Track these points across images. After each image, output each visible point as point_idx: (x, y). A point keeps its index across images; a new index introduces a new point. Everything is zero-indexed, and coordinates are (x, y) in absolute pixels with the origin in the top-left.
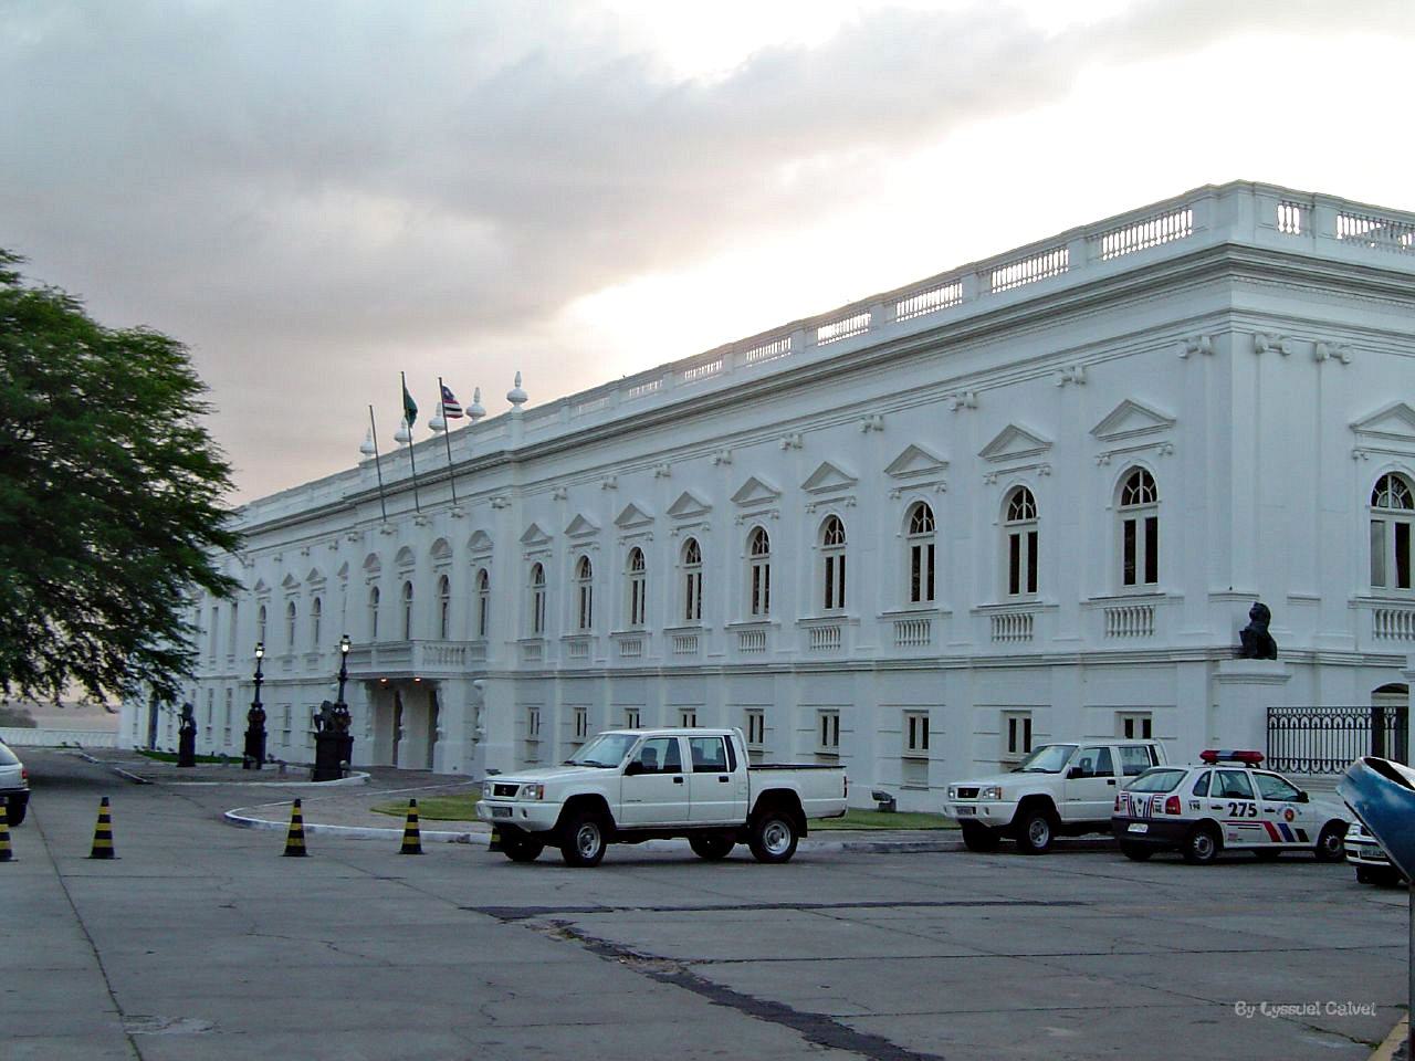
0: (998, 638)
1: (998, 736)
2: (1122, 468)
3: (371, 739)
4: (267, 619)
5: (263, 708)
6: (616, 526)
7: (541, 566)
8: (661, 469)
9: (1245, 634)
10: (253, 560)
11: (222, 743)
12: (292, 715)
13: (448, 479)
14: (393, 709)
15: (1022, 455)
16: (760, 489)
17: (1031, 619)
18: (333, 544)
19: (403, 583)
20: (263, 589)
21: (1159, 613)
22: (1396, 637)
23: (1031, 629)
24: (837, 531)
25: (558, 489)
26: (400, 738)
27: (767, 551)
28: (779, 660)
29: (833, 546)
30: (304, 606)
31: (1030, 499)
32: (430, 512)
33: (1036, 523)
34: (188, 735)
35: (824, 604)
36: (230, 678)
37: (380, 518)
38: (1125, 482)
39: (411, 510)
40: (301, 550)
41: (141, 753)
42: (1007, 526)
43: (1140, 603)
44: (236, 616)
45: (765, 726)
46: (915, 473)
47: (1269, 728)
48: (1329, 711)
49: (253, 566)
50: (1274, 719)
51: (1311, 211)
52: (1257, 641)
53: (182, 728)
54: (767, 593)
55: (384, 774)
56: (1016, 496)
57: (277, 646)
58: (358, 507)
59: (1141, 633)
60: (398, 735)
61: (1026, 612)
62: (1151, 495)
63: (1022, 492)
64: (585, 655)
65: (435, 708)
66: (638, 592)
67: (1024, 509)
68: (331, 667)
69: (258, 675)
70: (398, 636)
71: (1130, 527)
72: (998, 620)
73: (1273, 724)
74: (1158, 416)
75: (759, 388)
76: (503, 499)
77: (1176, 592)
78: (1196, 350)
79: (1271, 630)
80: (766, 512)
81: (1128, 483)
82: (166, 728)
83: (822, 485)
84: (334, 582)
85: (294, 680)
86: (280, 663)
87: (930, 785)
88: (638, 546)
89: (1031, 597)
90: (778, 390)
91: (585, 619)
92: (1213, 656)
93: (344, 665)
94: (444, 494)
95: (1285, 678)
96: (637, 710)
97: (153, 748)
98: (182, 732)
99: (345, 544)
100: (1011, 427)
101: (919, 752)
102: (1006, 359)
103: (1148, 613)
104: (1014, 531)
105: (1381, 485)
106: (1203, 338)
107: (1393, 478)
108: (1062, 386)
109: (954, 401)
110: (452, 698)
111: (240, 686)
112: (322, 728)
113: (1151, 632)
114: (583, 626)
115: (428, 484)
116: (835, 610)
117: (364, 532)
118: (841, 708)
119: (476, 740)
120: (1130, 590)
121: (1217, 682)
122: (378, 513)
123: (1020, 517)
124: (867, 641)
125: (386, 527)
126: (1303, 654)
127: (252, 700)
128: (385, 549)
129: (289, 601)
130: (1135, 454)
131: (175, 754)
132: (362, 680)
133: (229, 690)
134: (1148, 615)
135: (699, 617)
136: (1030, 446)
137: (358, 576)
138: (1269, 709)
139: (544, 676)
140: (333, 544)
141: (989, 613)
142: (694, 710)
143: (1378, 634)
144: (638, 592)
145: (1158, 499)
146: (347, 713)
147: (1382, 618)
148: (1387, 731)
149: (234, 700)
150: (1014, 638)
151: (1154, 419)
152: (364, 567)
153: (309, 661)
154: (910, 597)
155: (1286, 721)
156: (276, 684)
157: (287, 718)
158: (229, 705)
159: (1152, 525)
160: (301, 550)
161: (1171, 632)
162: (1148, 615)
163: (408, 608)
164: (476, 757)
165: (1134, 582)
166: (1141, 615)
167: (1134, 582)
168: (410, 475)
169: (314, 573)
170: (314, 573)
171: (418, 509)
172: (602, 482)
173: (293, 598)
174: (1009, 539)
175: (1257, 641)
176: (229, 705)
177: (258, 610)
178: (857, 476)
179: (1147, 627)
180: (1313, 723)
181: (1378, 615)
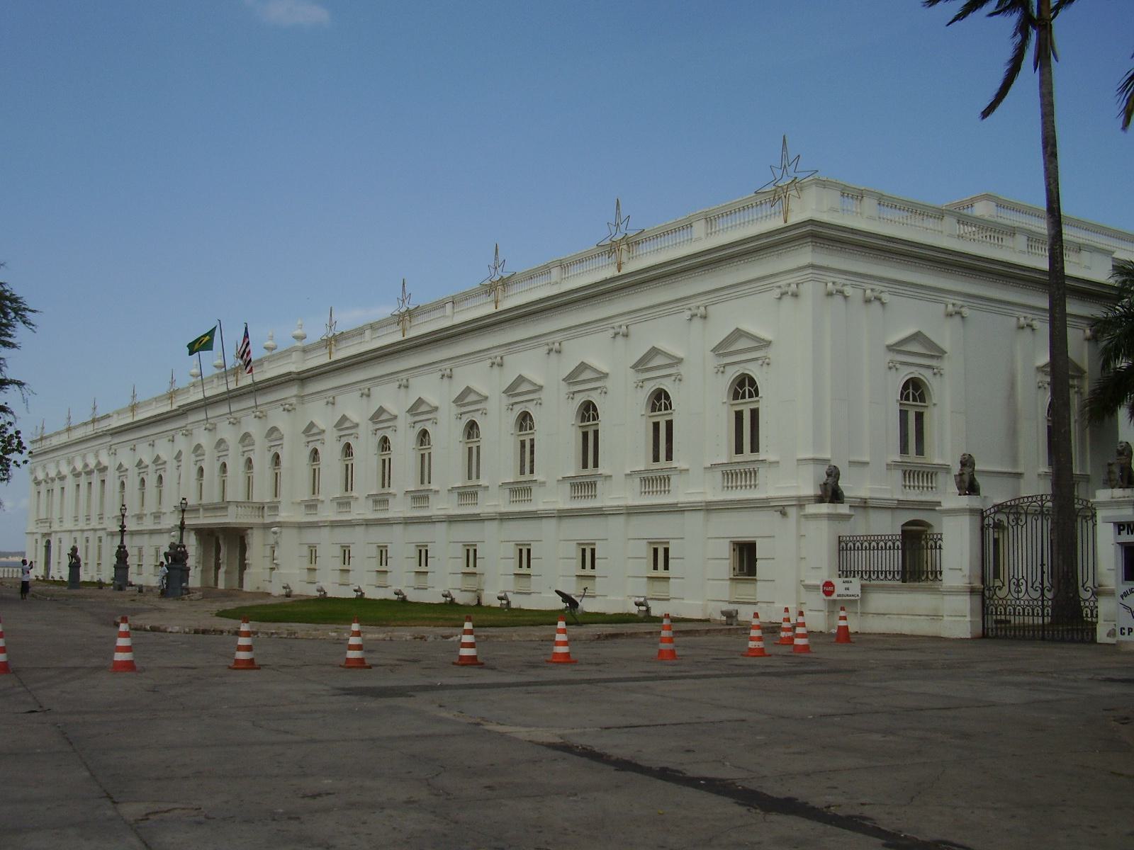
0: (645, 493)
1: (461, 560)
3: (199, 569)
4: (164, 483)
5: (126, 549)
7: (251, 460)
10: (115, 450)
11: (411, 579)
12: (144, 553)
13: (227, 399)
15: (347, 428)
19: (272, 454)
21: (761, 473)
22: (916, 488)
23: (669, 487)
24: (591, 412)
25: (329, 397)
26: (219, 568)
28: (486, 511)
29: (588, 423)
30: (151, 480)
31: (595, 409)
33: (672, 413)
34: (75, 566)
36: (87, 530)
40: (168, 438)
41: (41, 581)
42: (650, 417)
43: (747, 467)
44: (104, 488)
45: (477, 556)
46: (584, 381)
47: (839, 550)
48: (883, 538)
49: (333, 404)
50: (843, 544)
52: (832, 493)
53: (70, 563)
55: (209, 592)
56: (739, 382)
58: (188, 412)
59: (748, 487)
60: (218, 567)
63: (745, 378)
65: (243, 548)
67: (663, 404)
68: (172, 521)
69: (123, 526)
70: (216, 499)
72: (644, 480)
77: (684, 466)
78: (619, 333)
79: (840, 484)
81: (584, 410)
83: (466, 401)
84: (171, 464)
86: (135, 519)
87: (596, 594)
88: (387, 435)
89: (754, 457)
92: (800, 502)
93: (183, 518)
94: (224, 409)
95: (849, 517)
97: (48, 577)
98: (71, 566)
99: (179, 438)
104: (656, 420)
105: (906, 386)
106: (792, 285)
107: (913, 381)
109: (689, 313)
110: (256, 544)
112: (170, 561)
113: (755, 486)
114: (314, 493)
115: (263, 389)
116: (590, 470)
118: (429, 544)
119: (272, 569)
120: (739, 458)
121: (803, 519)
122: (251, 403)
124: (695, 486)
125: (232, 420)
127: (119, 543)
133: (36, 540)
134: (753, 475)
135: (352, 490)
137: (189, 461)
138: (839, 537)
139: (321, 524)
141: (457, 491)
142: (476, 545)
143: (905, 487)
146: (185, 551)
147: (907, 475)
148: (925, 551)
151: (757, 341)
152: (193, 453)
153: (155, 517)
155: (883, 544)
156: (133, 533)
157: (140, 556)
158: (100, 547)
160: (168, 438)
161: (608, 497)
162: (753, 475)
164: (272, 580)
165: (658, 461)
166: (730, 476)
167: (658, 461)
168: (225, 390)
169: (158, 458)
170: (158, 458)
171: (231, 413)
173: (144, 476)
174: (652, 425)
176: (100, 547)
178: (607, 371)
179: (753, 483)
180: (896, 545)
181: (905, 474)
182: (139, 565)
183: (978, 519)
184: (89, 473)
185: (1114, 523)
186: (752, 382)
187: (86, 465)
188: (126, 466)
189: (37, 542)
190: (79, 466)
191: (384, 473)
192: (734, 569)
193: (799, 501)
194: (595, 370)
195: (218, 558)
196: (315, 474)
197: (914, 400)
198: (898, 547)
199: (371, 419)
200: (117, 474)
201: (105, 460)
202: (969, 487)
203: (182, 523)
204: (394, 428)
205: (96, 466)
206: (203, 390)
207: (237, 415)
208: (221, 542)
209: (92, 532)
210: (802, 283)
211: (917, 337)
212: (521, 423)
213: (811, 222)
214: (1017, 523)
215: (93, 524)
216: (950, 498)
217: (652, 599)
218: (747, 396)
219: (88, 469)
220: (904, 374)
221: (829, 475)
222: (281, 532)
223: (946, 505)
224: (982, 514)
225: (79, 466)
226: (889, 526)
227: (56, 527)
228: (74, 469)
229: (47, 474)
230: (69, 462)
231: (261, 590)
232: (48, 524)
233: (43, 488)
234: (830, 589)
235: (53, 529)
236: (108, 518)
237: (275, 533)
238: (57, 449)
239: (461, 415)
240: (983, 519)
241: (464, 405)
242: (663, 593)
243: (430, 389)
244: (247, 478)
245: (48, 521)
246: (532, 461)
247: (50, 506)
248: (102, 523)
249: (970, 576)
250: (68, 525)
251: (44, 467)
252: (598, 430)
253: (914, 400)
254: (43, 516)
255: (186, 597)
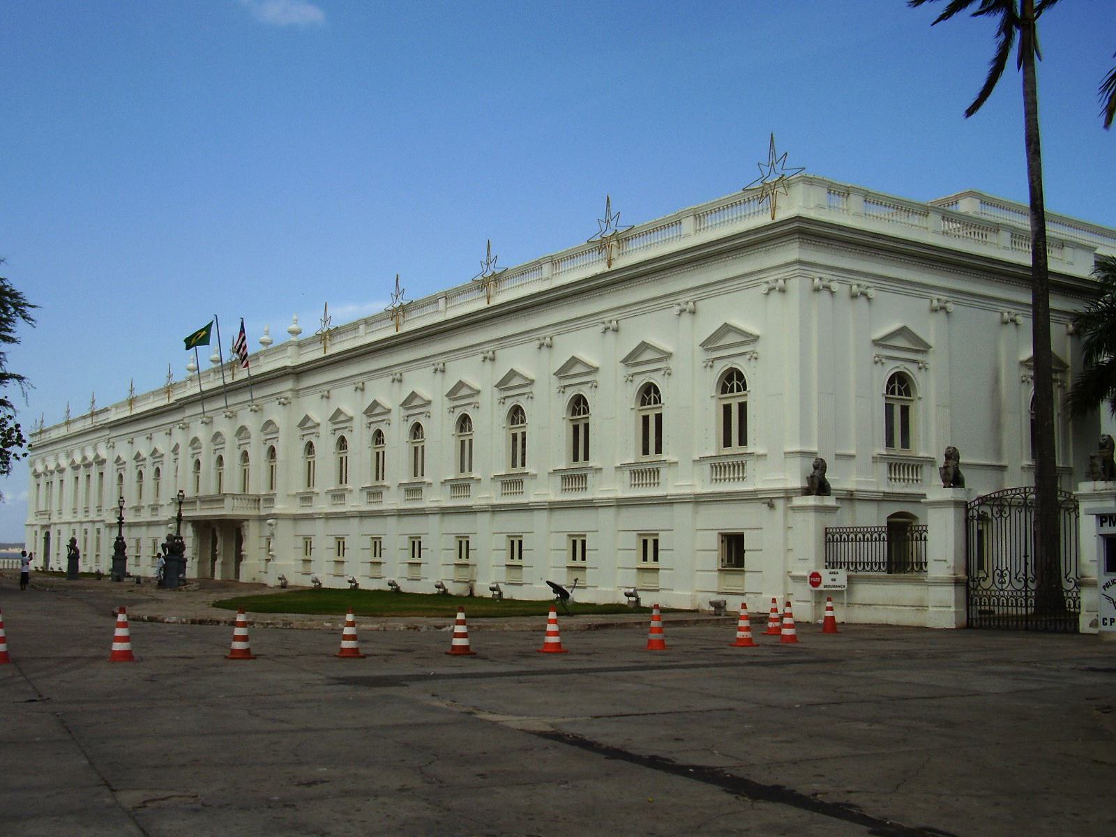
2: (719, 372)
5: (124, 540)
6: (364, 416)
7: (312, 443)
8: (324, 393)
9: (811, 479)
11: (404, 571)
14: (210, 541)
16: (649, 351)
17: (658, 472)
18: (149, 435)
20: (157, 455)
21: (662, 471)
22: (902, 481)
23: (658, 479)
26: (216, 560)
27: (346, 448)
30: (149, 473)
32: (234, 409)
35: (375, 478)
37: (200, 414)
38: (724, 378)
39: (247, 401)
42: (639, 410)
43: (735, 460)
46: (416, 407)
47: (826, 542)
50: (830, 536)
51: (847, 197)
54: (346, 476)
55: (205, 583)
57: (130, 502)
60: (214, 558)
61: (739, 460)
62: (658, 400)
63: (733, 373)
64: (420, 497)
65: (239, 540)
66: (343, 464)
68: (168, 513)
70: (213, 491)
71: (646, 419)
72: (634, 473)
73: (830, 539)
74: (663, 351)
75: (353, 353)
76: (286, 399)
77: (674, 459)
80: (470, 404)
82: (55, 556)
84: (169, 457)
85: (142, 522)
86: (132, 511)
89: (742, 450)
90: (131, 422)
91: (342, 478)
92: (788, 495)
93: (180, 510)
94: (220, 403)
96: (344, 538)
97: (47, 568)
98: (69, 557)
99: (177, 432)
100: (643, 343)
101: (516, 562)
102: (85, 440)
103: (583, 478)
105: (891, 381)
107: (898, 376)
108: (679, 315)
109: (678, 308)
110: (252, 536)
111: (106, 527)
112: (167, 553)
115: (258, 383)
116: (581, 463)
117: (188, 424)
119: (268, 560)
120: (728, 451)
123: (649, 404)
124: (684, 479)
125: (228, 413)
126: (845, 492)
128: (251, 421)
129: (155, 467)
130: (730, 359)
131: (62, 572)
132: (189, 521)
133: (36, 532)
134: (741, 467)
136: (523, 382)
137: (185, 452)
138: (826, 528)
139: (315, 517)
140: (149, 435)
143: (891, 479)
144: (343, 464)
145: (748, 389)
146: (182, 542)
149: (102, 535)
150: (576, 489)
152: (236, 436)
153: (153, 509)
154: (641, 452)
156: (131, 525)
157: (138, 547)
159: (659, 418)
161: (599, 489)
162: (741, 467)
163: (220, 473)
165: (578, 461)
167: (578, 461)
168: (222, 384)
169: (155, 451)
170: (155, 451)
172: (320, 394)
175: (818, 485)
176: (98, 539)
177: (154, 471)
179: (741, 475)
181: (890, 467)
182: (136, 556)
183: (962, 511)
184: (88, 466)
185: (1097, 515)
186: (740, 376)
187: (85, 458)
188: (124, 458)
189: (36, 534)
190: (78, 459)
191: (378, 466)
192: (722, 560)
193: (786, 493)
194: (585, 364)
195: (214, 550)
196: (310, 467)
197: (900, 394)
198: (884, 538)
199: (365, 413)
200: (115, 466)
201: (103, 453)
202: (953, 478)
203: (180, 515)
204: (388, 422)
205: (94, 459)
206: (200, 384)
207: (234, 409)
208: (217, 534)
209: (78, 524)
210: (790, 279)
211: (903, 332)
212: (513, 416)
213: (798, 218)
214: (1001, 516)
215: (92, 516)
216: (935, 490)
217: (641, 590)
218: (735, 390)
219: (87, 462)
220: (890, 369)
221: (816, 468)
222: (276, 524)
223: (931, 497)
224: (966, 506)
225: (78, 459)
226: (873, 518)
227: (55, 519)
228: (73, 462)
229: (47, 467)
230: (68, 455)
231: (257, 581)
232: (48, 517)
233: (42, 481)
234: (817, 580)
235: (52, 521)
236: (107, 510)
237: (271, 525)
238: (56, 442)
239: (454, 408)
240: (967, 511)
241: (456, 399)
242: (649, 583)
243: (423, 383)
244: (243, 471)
245: (47, 513)
246: (524, 454)
247: (49, 498)
248: (100, 515)
249: (955, 568)
250: (67, 517)
251: (44, 460)
252: (588, 424)
253: (900, 394)
254: (42, 508)
255: (183, 588)
